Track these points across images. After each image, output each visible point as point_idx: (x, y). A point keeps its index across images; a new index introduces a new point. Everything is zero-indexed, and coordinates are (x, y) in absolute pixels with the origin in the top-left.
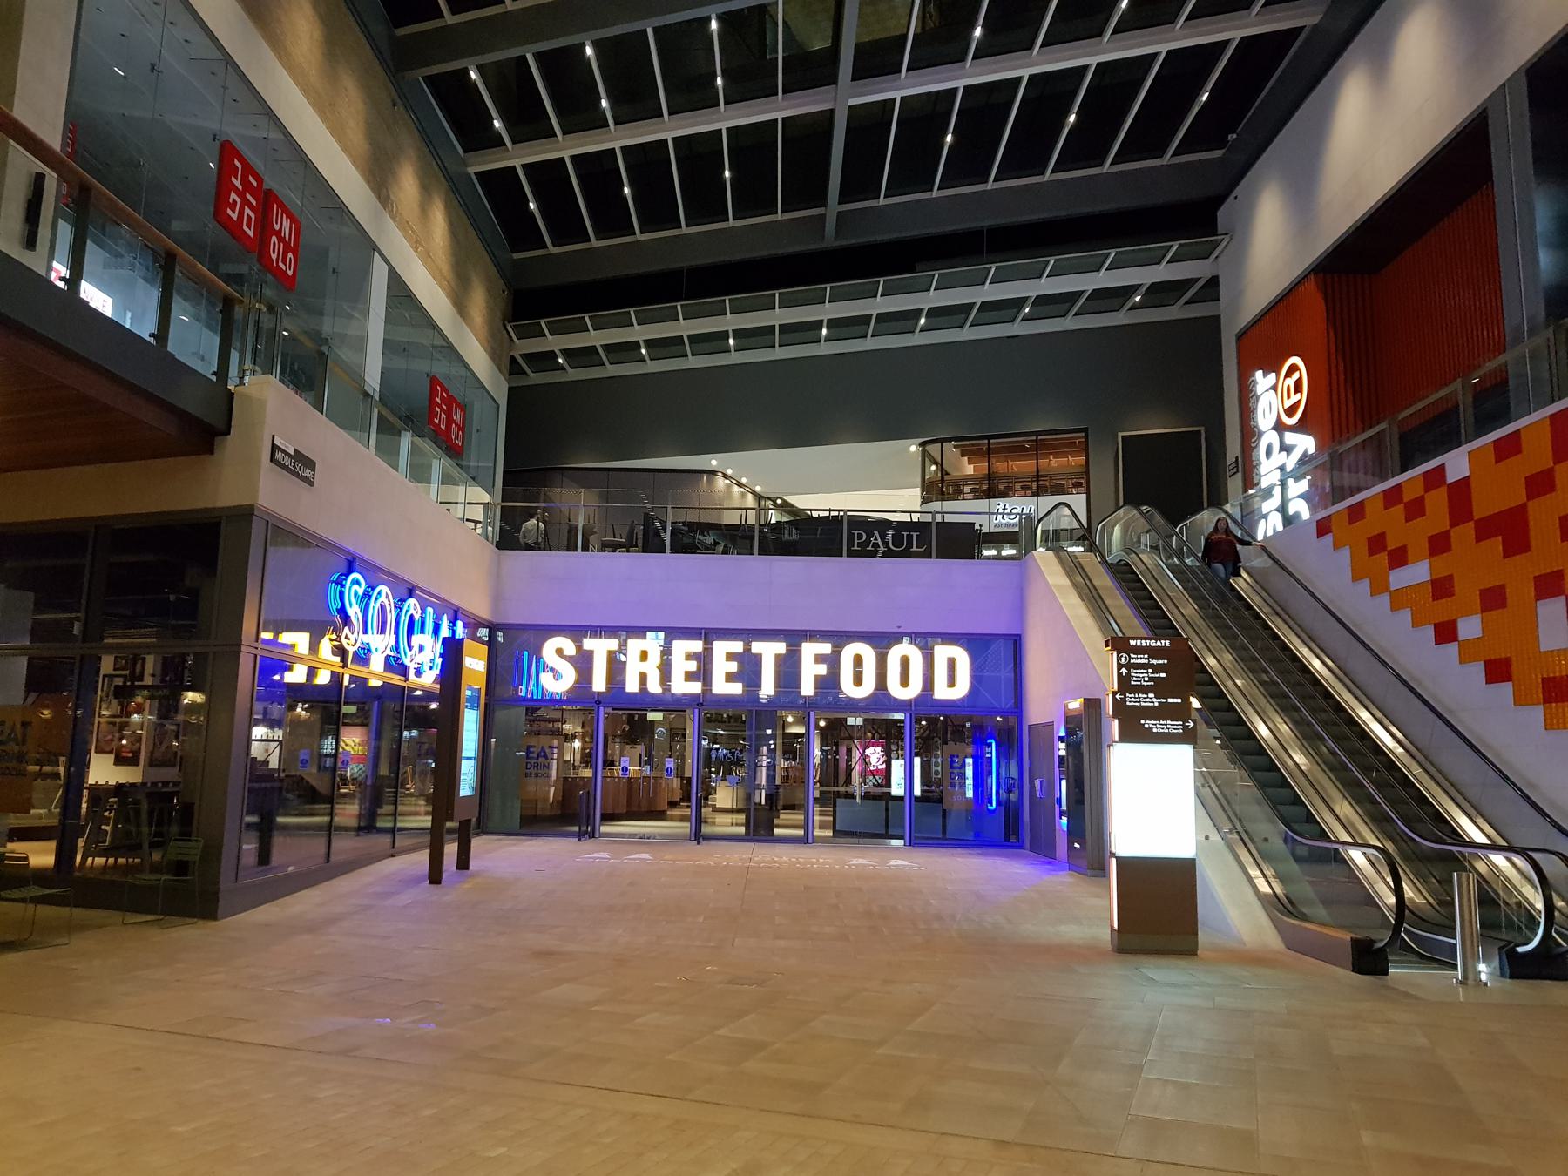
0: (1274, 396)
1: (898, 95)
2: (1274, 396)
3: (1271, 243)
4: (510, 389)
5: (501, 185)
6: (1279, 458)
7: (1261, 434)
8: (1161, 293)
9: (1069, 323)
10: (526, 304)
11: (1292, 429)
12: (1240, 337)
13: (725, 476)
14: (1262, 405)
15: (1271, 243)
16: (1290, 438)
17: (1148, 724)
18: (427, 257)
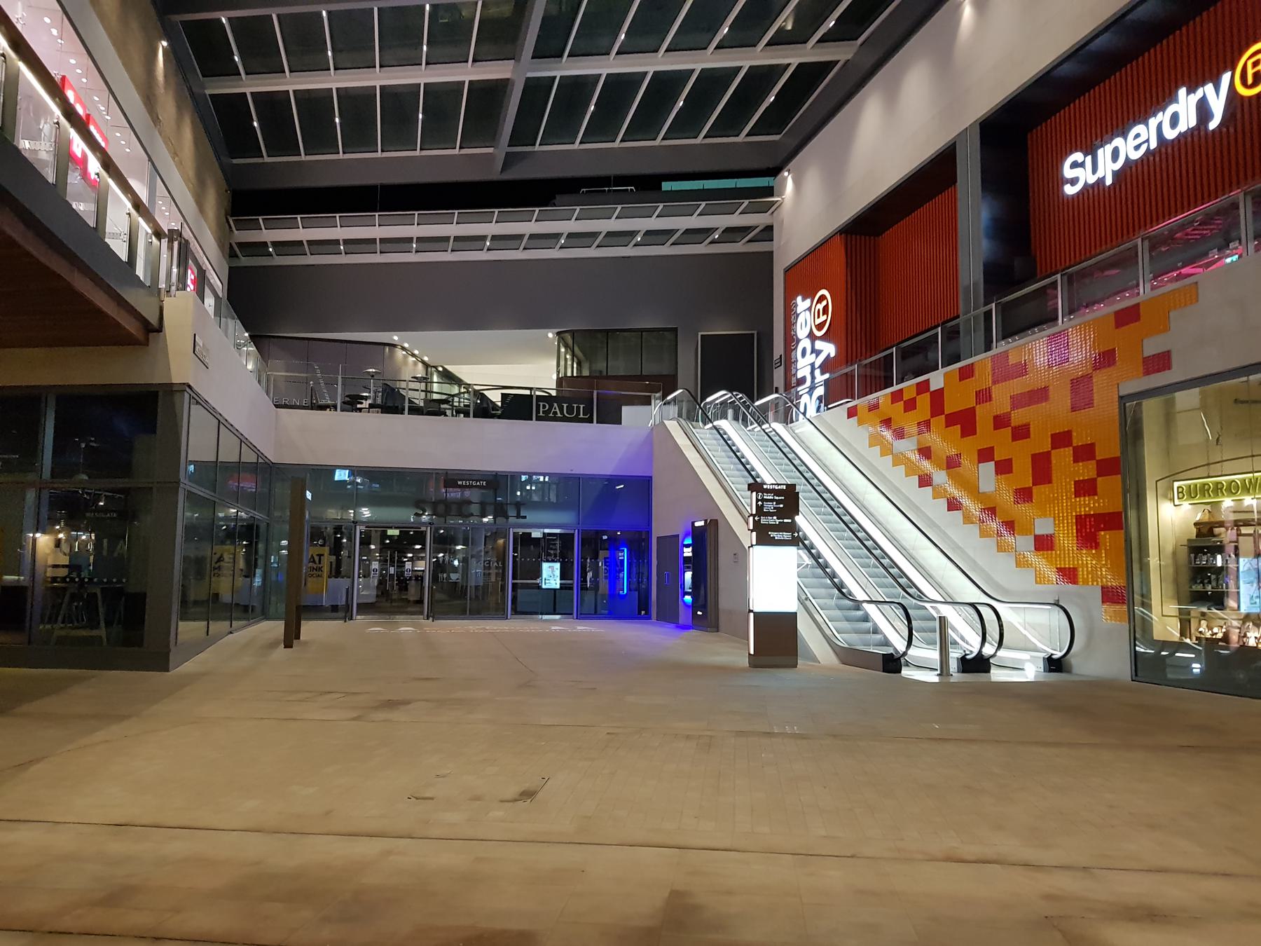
0: (808, 315)
1: (558, 74)
2: (808, 315)
3: (807, 206)
4: (230, 268)
5: (231, 108)
6: (810, 358)
7: (798, 341)
8: (732, 233)
9: (665, 250)
10: (246, 201)
11: (821, 338)
12: (787, 271)
13: (403, 348)
14: (801, 320)
15: (807, 206)
16: (819, 345)
17: (772, 534)
18: (180, 165)
